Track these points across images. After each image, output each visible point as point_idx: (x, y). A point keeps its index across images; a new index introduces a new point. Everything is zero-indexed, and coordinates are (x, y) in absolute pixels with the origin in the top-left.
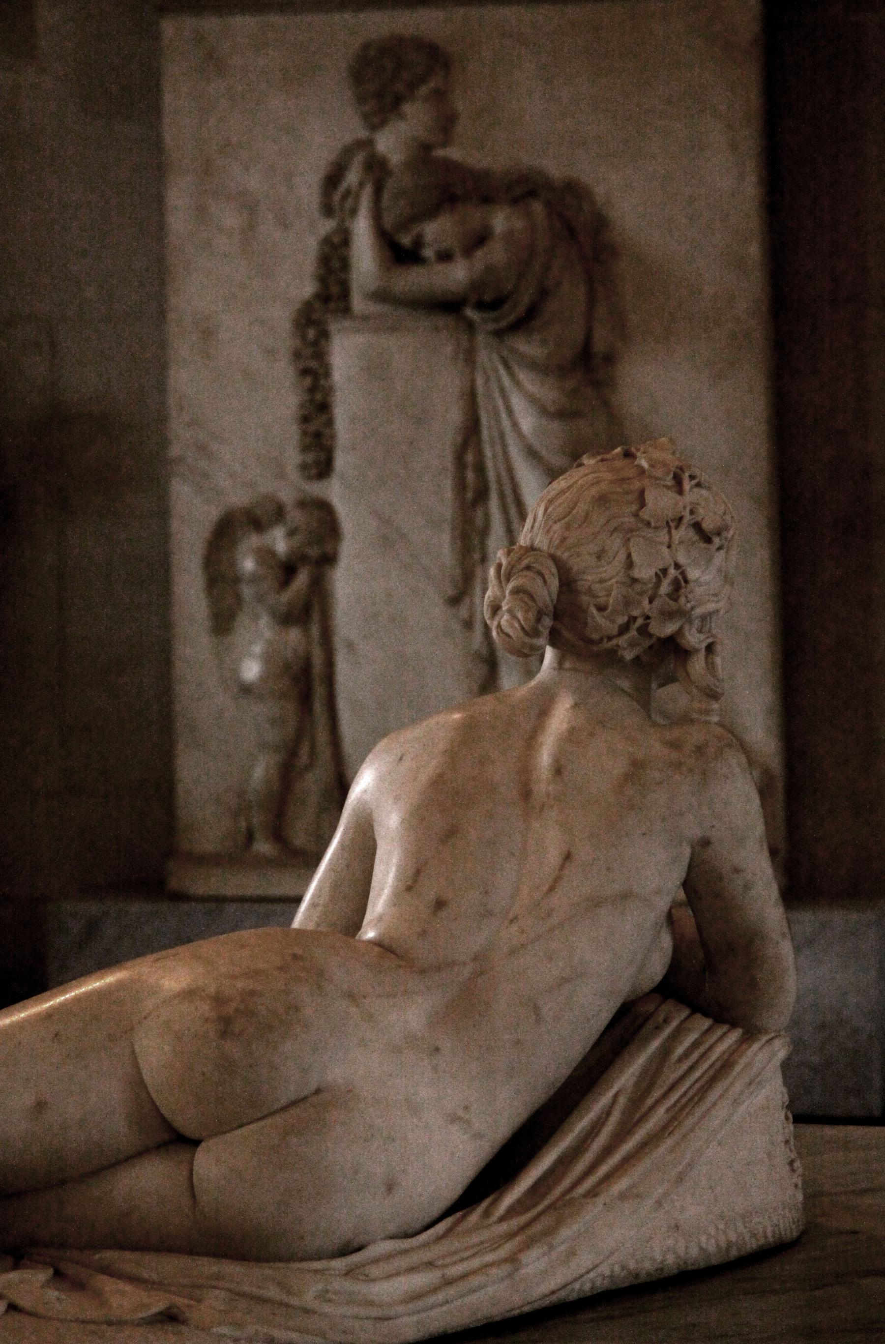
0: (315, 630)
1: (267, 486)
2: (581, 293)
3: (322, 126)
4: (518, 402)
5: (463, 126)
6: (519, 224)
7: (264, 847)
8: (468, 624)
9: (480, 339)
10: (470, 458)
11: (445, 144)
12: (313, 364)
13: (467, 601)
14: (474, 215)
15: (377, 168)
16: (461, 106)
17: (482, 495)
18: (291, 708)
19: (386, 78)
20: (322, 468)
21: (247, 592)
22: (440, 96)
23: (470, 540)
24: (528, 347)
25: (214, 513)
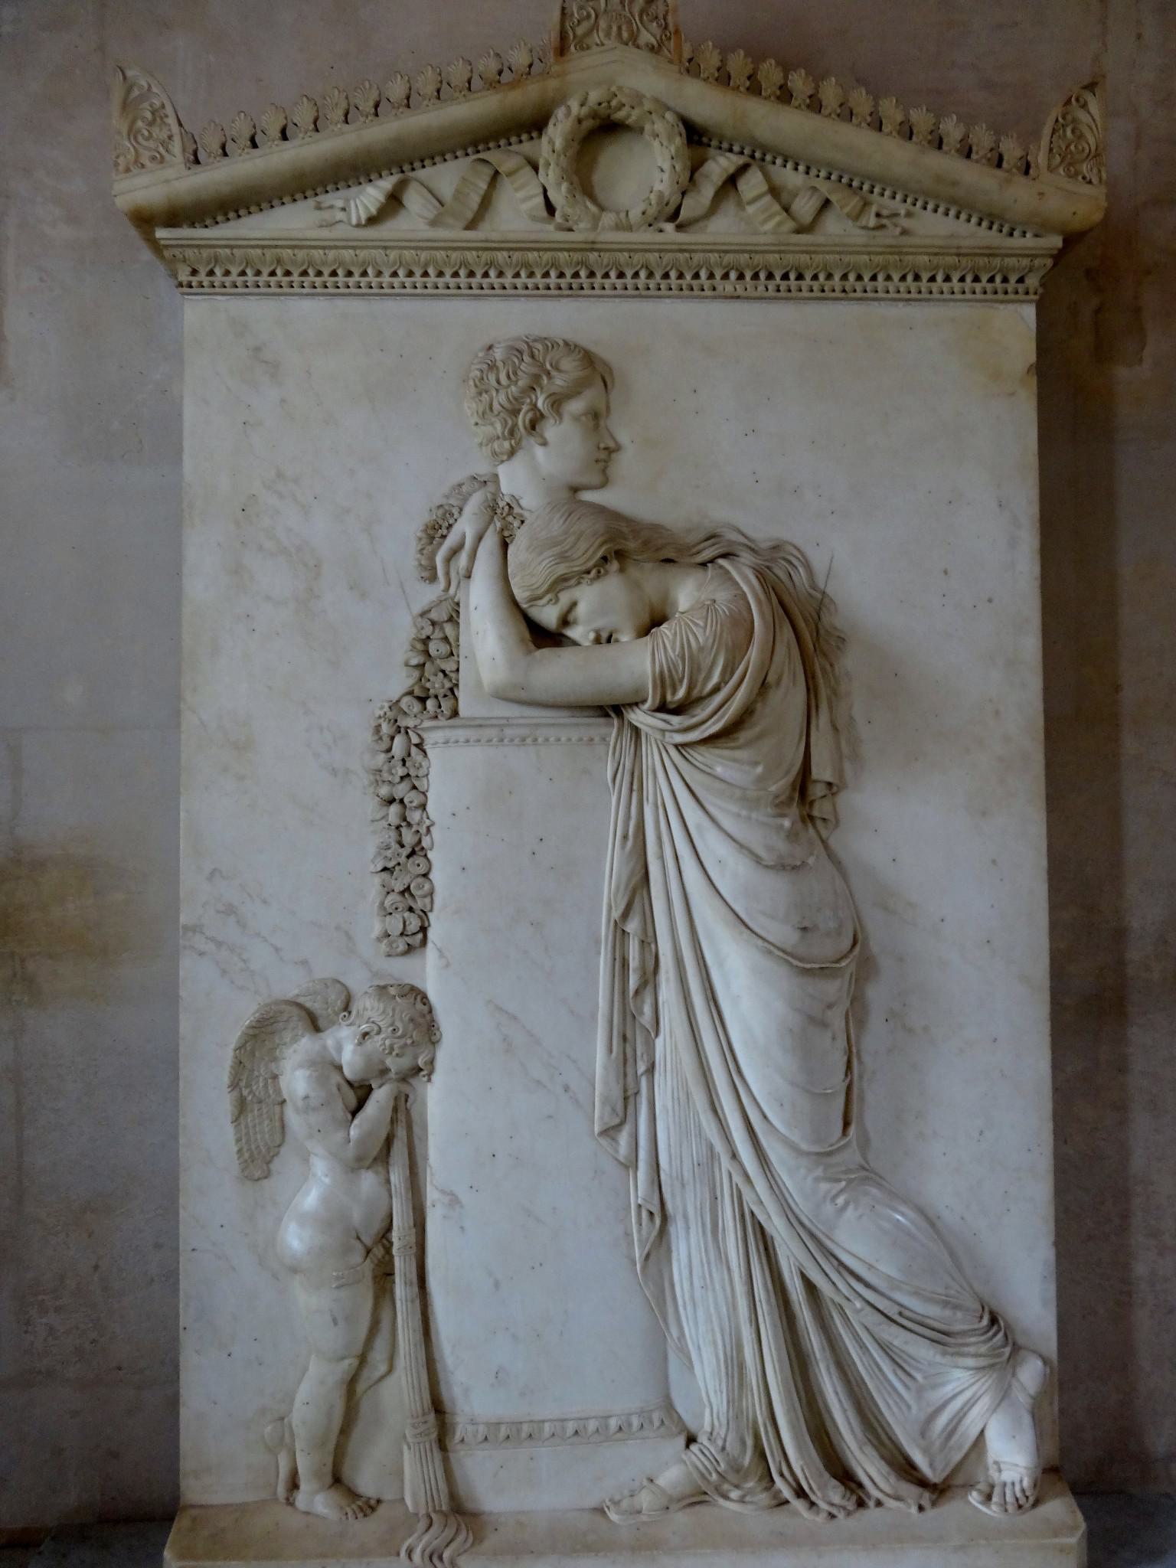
0: (398, 1176)
1: (326, 966)
5: (626, 464)
6: (723, 596)
8: (632, 1164)
9: (651, 756)
10: (633, 926)
11: (604, 483)
12: (401, 790)
13: (626, 1130)
14: (651, 579)
15: (503, 519)
16: (623, 436)
17: (650, 976)
20: (416, 939)
21: (295, 1120)
22: (596, 417)
23: (632, 1037)
25: (246, 1011)
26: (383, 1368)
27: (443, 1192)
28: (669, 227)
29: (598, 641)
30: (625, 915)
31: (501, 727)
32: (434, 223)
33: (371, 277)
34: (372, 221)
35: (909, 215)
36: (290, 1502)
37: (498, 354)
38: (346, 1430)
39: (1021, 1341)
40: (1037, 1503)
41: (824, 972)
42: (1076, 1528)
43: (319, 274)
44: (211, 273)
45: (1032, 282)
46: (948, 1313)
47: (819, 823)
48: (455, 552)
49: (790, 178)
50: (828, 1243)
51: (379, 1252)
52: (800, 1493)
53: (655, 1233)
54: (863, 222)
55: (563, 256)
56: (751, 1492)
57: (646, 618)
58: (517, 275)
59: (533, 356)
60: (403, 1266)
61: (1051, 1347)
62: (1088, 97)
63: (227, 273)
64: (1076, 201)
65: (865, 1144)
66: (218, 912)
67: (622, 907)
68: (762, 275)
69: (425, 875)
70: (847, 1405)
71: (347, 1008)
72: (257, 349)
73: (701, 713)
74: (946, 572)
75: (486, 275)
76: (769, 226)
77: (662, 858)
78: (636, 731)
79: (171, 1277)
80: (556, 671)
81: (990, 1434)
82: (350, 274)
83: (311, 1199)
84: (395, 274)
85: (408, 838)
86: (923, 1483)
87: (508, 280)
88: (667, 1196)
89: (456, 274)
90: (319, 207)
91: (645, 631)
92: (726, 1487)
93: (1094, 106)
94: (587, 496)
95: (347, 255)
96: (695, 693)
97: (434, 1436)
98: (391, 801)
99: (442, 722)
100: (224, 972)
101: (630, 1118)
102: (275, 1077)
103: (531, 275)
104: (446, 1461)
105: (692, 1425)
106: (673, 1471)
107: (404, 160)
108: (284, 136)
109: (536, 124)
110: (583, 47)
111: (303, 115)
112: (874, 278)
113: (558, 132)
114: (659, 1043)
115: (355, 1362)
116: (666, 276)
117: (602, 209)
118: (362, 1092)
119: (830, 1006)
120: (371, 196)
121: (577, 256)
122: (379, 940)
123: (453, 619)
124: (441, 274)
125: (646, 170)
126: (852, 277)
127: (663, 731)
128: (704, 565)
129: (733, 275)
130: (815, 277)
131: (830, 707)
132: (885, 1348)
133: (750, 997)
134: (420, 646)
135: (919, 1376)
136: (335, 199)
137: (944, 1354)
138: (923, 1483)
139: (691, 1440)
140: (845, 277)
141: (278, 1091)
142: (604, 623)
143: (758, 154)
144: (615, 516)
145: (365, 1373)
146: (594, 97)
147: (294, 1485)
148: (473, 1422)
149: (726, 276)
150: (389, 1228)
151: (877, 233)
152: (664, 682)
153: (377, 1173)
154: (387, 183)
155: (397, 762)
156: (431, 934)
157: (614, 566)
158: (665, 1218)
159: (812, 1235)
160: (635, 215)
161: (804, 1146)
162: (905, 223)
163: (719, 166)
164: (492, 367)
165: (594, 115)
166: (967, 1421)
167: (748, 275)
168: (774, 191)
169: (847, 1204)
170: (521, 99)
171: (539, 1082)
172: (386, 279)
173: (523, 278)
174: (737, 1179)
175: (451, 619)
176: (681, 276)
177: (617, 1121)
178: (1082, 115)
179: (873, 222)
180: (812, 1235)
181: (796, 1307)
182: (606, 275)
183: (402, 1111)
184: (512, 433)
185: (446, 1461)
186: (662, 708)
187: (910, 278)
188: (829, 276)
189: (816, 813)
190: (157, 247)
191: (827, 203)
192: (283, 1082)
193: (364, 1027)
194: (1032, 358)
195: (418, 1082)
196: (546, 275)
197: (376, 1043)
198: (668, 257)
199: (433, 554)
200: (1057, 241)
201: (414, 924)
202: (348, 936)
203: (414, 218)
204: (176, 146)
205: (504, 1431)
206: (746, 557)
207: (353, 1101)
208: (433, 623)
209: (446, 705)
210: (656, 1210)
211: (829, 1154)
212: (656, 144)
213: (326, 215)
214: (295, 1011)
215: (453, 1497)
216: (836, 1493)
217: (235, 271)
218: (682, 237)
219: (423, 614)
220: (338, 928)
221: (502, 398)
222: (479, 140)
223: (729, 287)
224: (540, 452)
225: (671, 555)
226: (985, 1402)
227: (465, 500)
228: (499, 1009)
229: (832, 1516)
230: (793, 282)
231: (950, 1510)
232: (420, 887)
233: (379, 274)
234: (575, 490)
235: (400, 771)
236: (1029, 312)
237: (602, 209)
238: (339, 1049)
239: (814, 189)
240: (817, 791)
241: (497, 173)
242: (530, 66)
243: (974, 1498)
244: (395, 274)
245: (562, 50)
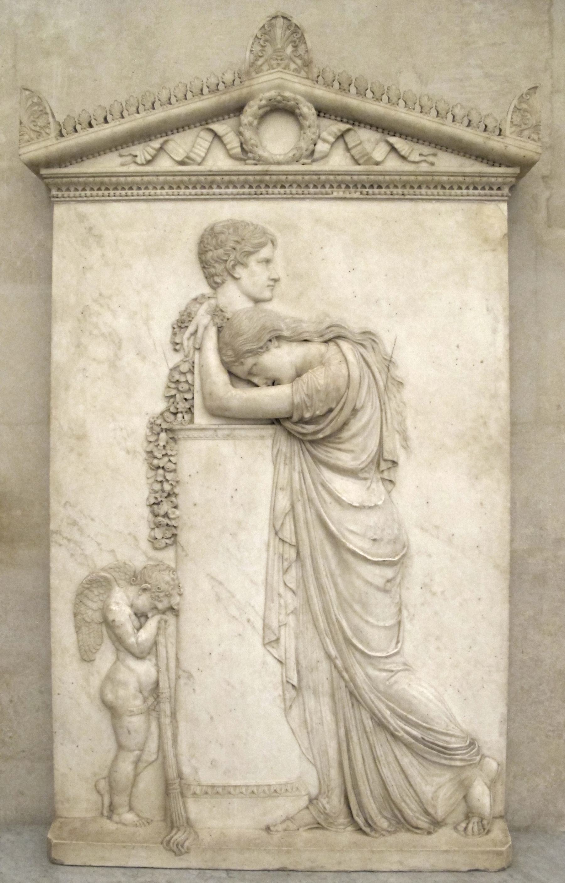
42: (82, 218)
61: (502, 757)
66: (166, 497)
72: (90, 229)
74: (458, 347)
98: (158, 467)
100: (72, 555)
109: (238, 109)
153: (150, 660)
171: (234, 617)
190: (42, 177)
220: (130, 534)
228: (213, 578)
236: (504, 206)
242: (234, 81)
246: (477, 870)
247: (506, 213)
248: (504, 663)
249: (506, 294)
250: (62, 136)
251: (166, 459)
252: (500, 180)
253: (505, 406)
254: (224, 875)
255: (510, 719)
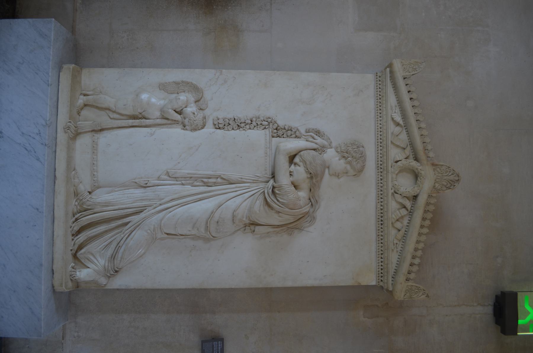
0: (159, 121)
2: (277, 223)
3: (337, 132)
4: (239, 200)
6: (302, 203)
7: (81, 100)
8: (159, 178)
9: (262, 185)
12: (254, 123)
13: (168, 178)
14: (305, 185)
15: (320, 150)
18: (129, 111)
19: (352, 154)
24: (259, 204)
26: (112, 117)
27: (154, 132)
28: (393, 191)
29: (290, 172)
30: (222, 178)
31: (269, 148)
32: (392, 133)
33: (380, 119)
34: (393, 119)
35: (397, 251)
36: (81, 94)
37: (361, 149)
38: (97, 107)
39: (111, 279)
40: (71, 280)
41: (207, 228)
43: (380, 106)
44: (380, 81)
45: (381, 284)
46: (119, 259)
47: (244, 228)
48: (313, 138)
49: (406, 221)
50: (138, 228)
51: (140, 116)
52: (77, 219)
53: (142, 185)
54: (395, 240)
55: (385, 165)
56: (77, 208)
57: (296, 184)
58: (381, 154)
59: (360, 157)
60: (136, 122)
61: (109, 287)
62: (425, 295)
63: (380, 84)
64: (400, 295)
65: (162, 239)
67: (224, 177)
68: (382, 215)
69: (233, 129)
70: (97, 232)
71: (201, 109)
73: (273, 197)
75: (381, 146)
76: (393, 216)
77: (236, 187)
78: (268, 182)
79: (134, 66)
80: (283, 161)
81: (88, 269)
82: (380, 113)
83: (153, 100)
84: (380, 124)
85: (242, 125)
86: (77, 252)
87: (379, 152)
88: (151, 188)
89: (381, 139)
90: (395, 106)
91: (293, 183)
92: (79, 201)
93: (424, 296)
94: (327, 170)
95: (384, 113)
96: (277, 195)
97: (95, 129)
98: (252, 121)
99: (271, 134)
100: (210, 80)
101: (171, 179)
102: (184, 92)
103: (381, 157)
104: (89, 132)
105: (93, 193)
106: (83, 188)
107: (407, 127)
108: (411, 99)
109: (416, 159)
110: (434, 170)
111: (416, 103)
112: (382, 243)
113: (414, 164)
114: (189, 186)
115: (114, 110)
116: (381, 191)
117: (397, 175)
118: (180, 113)
119: (198, 229)
120: (399, 119)
121: (385, 168)
122: (217, 117)
123: (296, 137)
124: (381, 135)
125: (405, 184)
126: (382, 237)
127: (268, 188)
128: (310, 199)
129: (382, 207)
130: (382, 228)
131: (274, 231)
132: (110, 243)
133: (201, 208)
134: (290, 128)
135: (103, 252)
136: (398, 110)
137: (109, 258)
138: (77, 252)
139: (90, 193)
140: (382, 236)
141: (181, 92)
142: (295, 174)
143: (411, 213)
144: (322, 178)
145: (111, 112)
146: (423, 172)
147: (85, 95)
148: (98, 138)
149: (382, 206)
150: (146, 119)
151: (392, 244)
152: (280, 187)
154: (401, 122)
155: (261, 122)
156: (218, 130)
157: (309, 176)
158: (145, 187)
159: (140, 224)
160: (396, 183)
161: (163, 222)
162: (395, 250)
163: (408, 204)
164: (358, 147)
165: (418, 173)
166: (91, 264)
167: (382, 211)
168: (402, 217)
169: (148, 233)
170: (421, 155)
172: (379, 122)
173: (380, 156)
174: (155, 205)
175: (296, 136)
176: (381, 194)
177: (170, 175)
178: (421, 294)
179: (395, 242)
180: (140, 224)
181: (122, 220)
182: (381, 176)
183: (175, 122)
184: (342, 152)
185: (89, 132)
186: (274, 187)
187: (382, 252)
188: (382, 232)
189: (247, 227)
190: (386, 68)
191: (399, 230)
192: (183, 93)
193: (196, 113)
194: (362, 284)
195: (181, 126)
196: (381, 161)
197: (192, 116)
198: (385, 191)
199: (311, 132)
200: (391, 289)
201: (221, 126)
202: (218, 110)
203: (392, 128)
204: (407, 74)
205: (95, 146)
206: (312, 210)
207: (177, 110)
208: (295, 132)
209: (275, 135)
210: (147, 185)
211: (161, 229)
212: (412, 188)
213: (394, 108)
214: (200, 97)
215: (80, 133)
216: (76, 228)
217: (380, 86)
218: (390, 194)
219: (298, 129)
221: (350, 149)
222: (412, 144)
223: (379, 206)
224: (337, 158)
225: (312, 191)
226: (96, 268)
227: (325, 140)
229: (71, 227)
230: (380, 222)
231: (70, 257)
232: (230, 128)
233: (380, 120)
234: (328, 167)
235: (259, 123)
236: (374, 283)
237: (397, 175)
238: (191, 107)
239: (402, 227)
240: (252, 227)
241: (405, 149)
243: (73, 264)
244: (380, 124)
245: (433, 165)
246: (53, 273)
247: (370, 284)
248: (156, 286)
249: (333, 285)
250: (404, 79)
251: (255, 124)
252: (386, 281)
253: (280, 285)
254: (54, 150)
255: (127, 291)
